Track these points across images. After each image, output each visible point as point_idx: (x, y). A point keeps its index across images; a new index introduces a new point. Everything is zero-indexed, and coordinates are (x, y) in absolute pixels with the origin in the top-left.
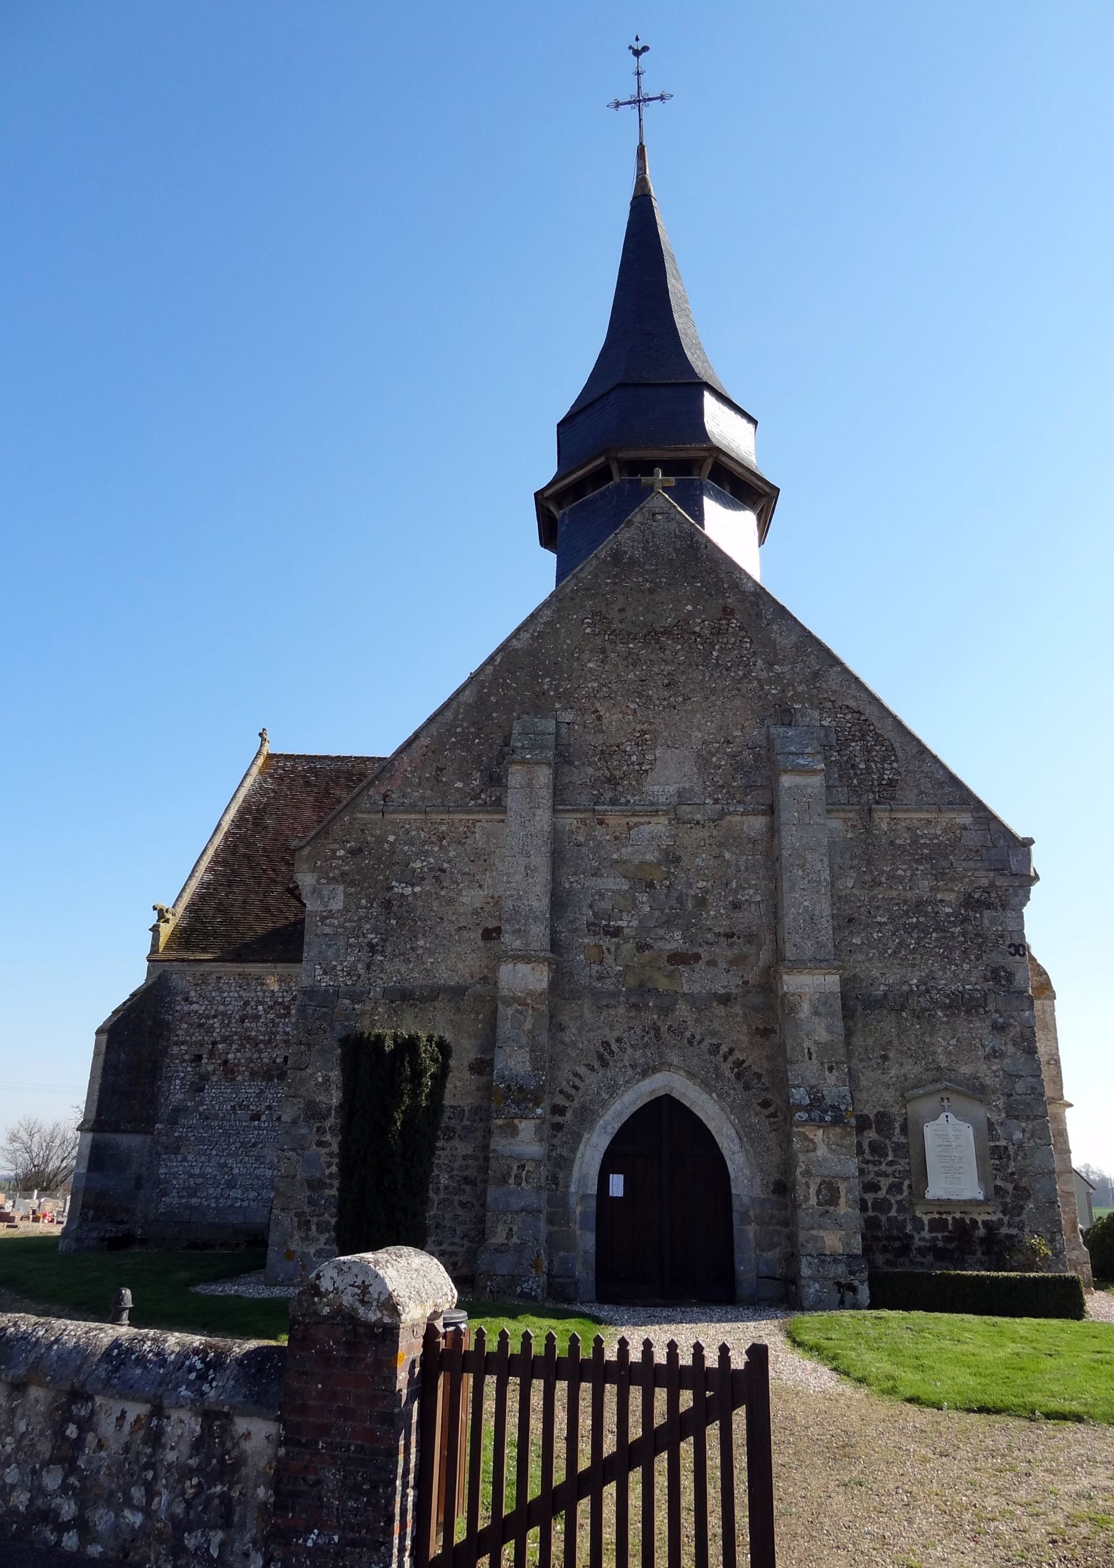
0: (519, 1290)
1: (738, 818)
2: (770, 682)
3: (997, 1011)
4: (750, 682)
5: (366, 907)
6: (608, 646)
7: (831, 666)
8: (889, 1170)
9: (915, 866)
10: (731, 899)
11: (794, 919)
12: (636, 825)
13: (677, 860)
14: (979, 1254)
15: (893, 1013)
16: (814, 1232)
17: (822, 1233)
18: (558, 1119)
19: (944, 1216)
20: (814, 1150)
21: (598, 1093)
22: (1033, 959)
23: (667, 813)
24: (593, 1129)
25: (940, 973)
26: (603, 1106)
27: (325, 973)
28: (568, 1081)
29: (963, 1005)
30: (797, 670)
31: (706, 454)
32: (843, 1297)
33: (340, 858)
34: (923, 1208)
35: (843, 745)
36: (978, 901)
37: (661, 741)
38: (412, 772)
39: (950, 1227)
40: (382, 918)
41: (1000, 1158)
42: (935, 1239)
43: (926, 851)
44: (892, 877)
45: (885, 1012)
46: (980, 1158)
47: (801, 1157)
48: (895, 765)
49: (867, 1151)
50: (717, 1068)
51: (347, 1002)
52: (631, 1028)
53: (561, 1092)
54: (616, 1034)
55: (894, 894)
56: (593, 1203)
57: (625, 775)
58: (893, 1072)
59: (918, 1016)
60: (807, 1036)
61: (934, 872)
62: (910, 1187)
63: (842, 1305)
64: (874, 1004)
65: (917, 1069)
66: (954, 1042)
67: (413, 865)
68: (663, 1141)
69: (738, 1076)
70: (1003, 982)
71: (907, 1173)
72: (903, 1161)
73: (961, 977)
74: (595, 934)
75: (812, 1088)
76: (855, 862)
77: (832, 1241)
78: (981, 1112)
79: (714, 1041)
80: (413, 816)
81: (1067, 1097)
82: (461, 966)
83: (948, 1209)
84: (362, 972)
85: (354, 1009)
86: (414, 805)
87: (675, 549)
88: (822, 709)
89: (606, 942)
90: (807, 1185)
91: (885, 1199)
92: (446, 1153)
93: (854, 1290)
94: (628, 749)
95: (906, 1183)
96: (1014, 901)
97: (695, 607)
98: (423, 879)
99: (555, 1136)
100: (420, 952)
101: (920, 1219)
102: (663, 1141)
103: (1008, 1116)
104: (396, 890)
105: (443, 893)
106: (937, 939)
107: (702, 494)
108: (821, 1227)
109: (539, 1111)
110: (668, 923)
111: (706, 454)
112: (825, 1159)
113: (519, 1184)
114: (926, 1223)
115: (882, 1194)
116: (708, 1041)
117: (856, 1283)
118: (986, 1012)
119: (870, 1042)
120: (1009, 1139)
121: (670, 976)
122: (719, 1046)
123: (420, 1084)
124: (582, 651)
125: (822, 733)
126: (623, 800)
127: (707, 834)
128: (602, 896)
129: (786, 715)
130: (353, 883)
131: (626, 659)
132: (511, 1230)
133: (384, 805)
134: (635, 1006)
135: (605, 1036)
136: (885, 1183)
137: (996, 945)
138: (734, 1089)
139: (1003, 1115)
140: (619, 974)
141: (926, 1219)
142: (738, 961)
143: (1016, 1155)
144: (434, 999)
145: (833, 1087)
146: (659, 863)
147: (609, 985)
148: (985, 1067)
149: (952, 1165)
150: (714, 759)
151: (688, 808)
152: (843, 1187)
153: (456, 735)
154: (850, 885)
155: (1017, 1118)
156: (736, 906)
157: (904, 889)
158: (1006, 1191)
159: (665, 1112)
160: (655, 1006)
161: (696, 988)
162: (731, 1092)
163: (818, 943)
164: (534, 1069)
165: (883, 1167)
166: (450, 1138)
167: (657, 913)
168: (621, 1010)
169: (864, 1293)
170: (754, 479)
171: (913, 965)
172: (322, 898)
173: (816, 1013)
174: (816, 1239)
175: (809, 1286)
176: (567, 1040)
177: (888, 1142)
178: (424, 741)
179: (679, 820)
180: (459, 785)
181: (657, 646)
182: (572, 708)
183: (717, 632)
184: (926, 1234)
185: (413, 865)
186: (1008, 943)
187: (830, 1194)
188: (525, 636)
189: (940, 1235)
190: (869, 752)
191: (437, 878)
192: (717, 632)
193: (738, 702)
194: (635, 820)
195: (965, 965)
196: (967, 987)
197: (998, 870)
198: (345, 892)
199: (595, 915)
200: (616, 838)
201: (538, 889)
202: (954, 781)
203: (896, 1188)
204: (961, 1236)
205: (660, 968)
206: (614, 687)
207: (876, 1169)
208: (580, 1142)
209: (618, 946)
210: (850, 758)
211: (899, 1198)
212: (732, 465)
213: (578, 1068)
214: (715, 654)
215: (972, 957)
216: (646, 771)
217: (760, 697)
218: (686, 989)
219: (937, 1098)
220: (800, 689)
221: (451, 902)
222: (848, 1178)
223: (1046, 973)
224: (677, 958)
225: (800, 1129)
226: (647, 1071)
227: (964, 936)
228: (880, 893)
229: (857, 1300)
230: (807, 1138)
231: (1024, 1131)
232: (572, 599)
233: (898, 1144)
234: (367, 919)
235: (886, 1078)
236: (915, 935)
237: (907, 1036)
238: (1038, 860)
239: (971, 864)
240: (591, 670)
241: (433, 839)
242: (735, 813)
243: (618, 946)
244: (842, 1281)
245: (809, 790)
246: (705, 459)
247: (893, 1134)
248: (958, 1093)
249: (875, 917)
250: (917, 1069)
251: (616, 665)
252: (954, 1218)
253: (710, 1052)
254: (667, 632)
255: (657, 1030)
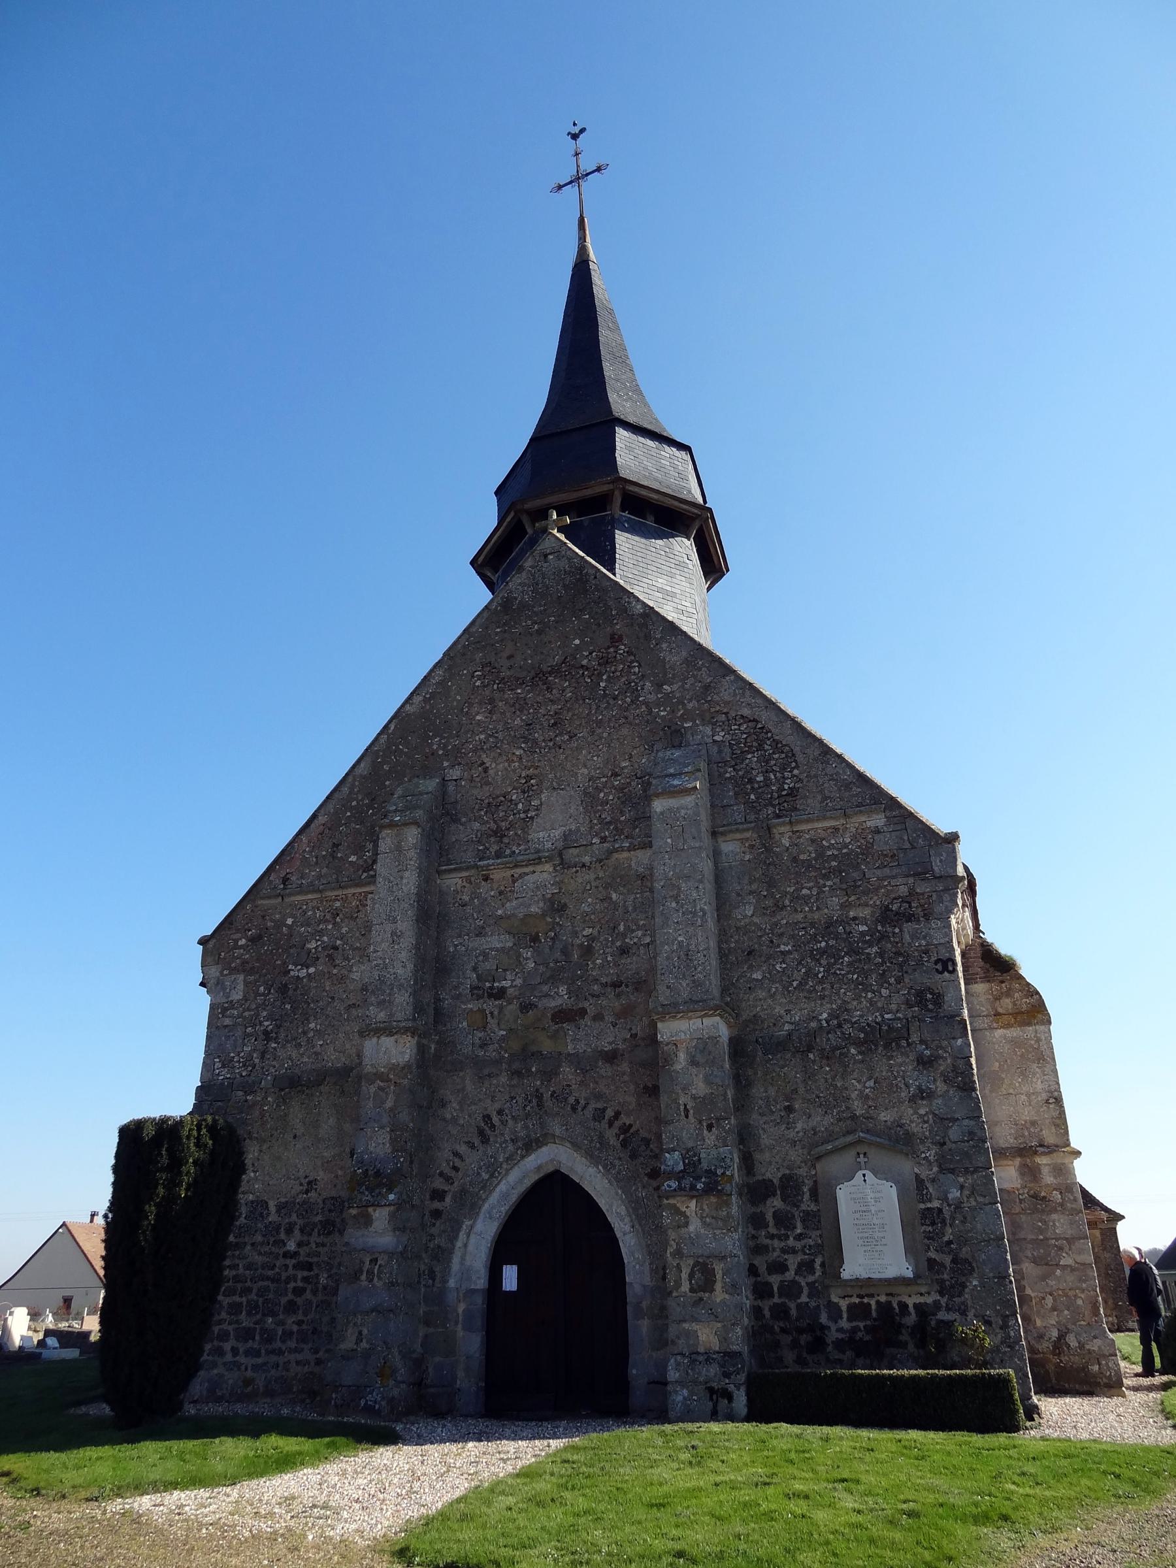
0: (363, 1402)
1: (625, 854)
2: (658, 704)
3: (922, 1042)
4: (638, 707)
5: (263, 994)
6: (497, 695)
7: (724, 676)
8: (798, 1245)
9: (822, 882)
10: (618, 944)
11: (668, 958)
12: (521, 876)
13: (563, 907)
14: (911, 1347)
15: (798, 1056)
16: (686, 1326)
17: (695, 1326)
18: (437, 1205)
19: (866, 1300)
20: (687, 1224)
21: (478, 1173)
22: (1021, 978)
23: (550, 859)
24: (478, 1214)
25: (855, 1003)
26: (483, 1188)
27: (223, 1066)
28: (448, 1161)
29: (883, 1038)
30: (687, 686)
31: (611, 487)
32: (716, 1406)
33: (241, 947)
34: (840, 1291)
35: (739, 758)
36: (897, 914)
37: (546, 784)
38: (310, 852)
39: (874, 1314)
40: (278, 1003)
41: (933, 1224)
42: (855, 1330)
43: (834, 864)
44: (796, 898)
45: (789, 1056)
46: (907, 1226)
47: (672, 1235)
48: (796, 772)
49: (771, 1223)
50: (601, 1136)
51: (240, 1093)
52: (513, 1098)
53: (441, 1174)
54: (497, 1106)
55: (800, 917)
56: (479, 1300)
57: (511, 826)
58: (799, 1126)
59: (827, 1057)
60: (683, 1089)
61: (844, 886)
62: (823, 1265)
63: (714, 1416)
64: (779, 1046)
65: (829, 1120)
66: (871, 1083)
67: (308, 946)
68: (554, 1222)
69: (624, 1144)
70: (930, 1006)
71: (819, 1249)
72: (815, 1234)
73: (879, 1005)
74: (479, 997)
75: (688, 1151)
76: (754, 887)
77: (707, 1336)
78: (908, 1167)
79: (599, 1105)
80: (310, 896)
81: (1075, 1143)
82: (348, 1046)
83: (871, 1291)
84: (257, 1061)
85: (246, 1101)
86: (312, 884)
87: (564, 586)
88: (714, 724)
89: (490, 1005)
90: (679, 1267)
91: (794, 1282)
92: (326, 1249)
93: (730, 1397)
94: (514, 797)
95: (818, 1261)
96: (939, 908)
97: (582, 641)
98: (318, 959)
99: (434, 1225)
100: (311, 1034)
101: (837, 1304)
102: (554, 1222)
103: (942, 1170)
104: (292, 973)
105: (335, 971)
106: (850, 964)
107: (614, 528)
108: (694, 1319)
109: (391, 1197)
110: (553, 978)
111: (611, 487)
112: (698, 1236)
113: (371, 1281)
114: (844, 1308)
115: (790, 1275)
116: (593, 1105)
117: (731, 1387)
118: (909, 1045)
119: (772, 1092)
120: (945, 1199)
121: (554, 1036)
122: (604, 1110)
123: (180, 1173)
124: (471, 705)
125: (715, 749)
126: (508, 852)
127: (593, 876)
128: (485, 955)
129: (675, 736)
130: (251, 971)
131: (513, 705)
132: (360, 1333)
133: (284, 889)
134: (518, 1073)
135: (486, 1109)
136: (793, 1262)
137: (920, 963)
138: (620, 1159)
139: (935, 1169)
140: (503, 1038)
141: (844, 1304)
142: (626, 1012)
143: (953, 1218)
144: (319, 1083)
145: (714, 1147)
146: (544, 915)
147: (491, 1052)
148: (911, 1111)
149: (873, 1233)
150: (602, 795)
151: (575, 851)
152: (719, 1268)
153: (351, 808)
154: (750, 913)
155: (952, 1171)
156: (624, 951)
157: (811, 910)
158: (943, 1265)
159: (555, 1189)
160: (538, 1071)
161: (581, 1047)
162: (617, 1162)
163: (694, 981)
164: (395, 1150)
165: (791, 1242)
166: (329, 1233)
167: (542, 969)
168: (503, 1079)
169: (741, 1401)
170: (676, 503)
171: (822, 998)
172: (224, 989)
173: (693, 1062)
174: (689, 1334)
175: (676, 1392)
176: (448, 1116)
177: (790, 1212)
178: (322, 819)
179: (564, 865)
180: (353, 858)
181: (545, 687)
182: (459, 764)
183: (605, 661)
184: (844, 1323)
185: (308, 946)
186: (933, 959)
187: (704, 1278)
188: (417, 699)
189: (861, 1325)
190: (767, 762)
191: (330, 957)
192: (605, 661)
193: (625, 731)
194: (519, 871)
195: (883, 991)
196: (886, 1016)
197: (920, 874)
198: (245, 981)
199: (479, 977)
200: (501, 893)
201: (404, 955)
202: (863, 780)
203: (806, 1267)
204: (884, 1324)
205: (544, 1029)
206: (500, 736)
207: (783, 1244)
208: (459, 1230)
209: (501, 1008)
210: (747, 772)
211: (811, 1279)
212: (644, 493)
213: (458, 1147)
214: (602, 684)
215: (892, 980)
216: (532, 818)
217: (647, 722)
218: (570, 1049)
219: (853, 1153)
220: (690, 706)
221: (342, 979)
222: (724, 1258)
223: (1038, 993)
224: (563, 1016)
225: (672, 1201)
226: (530, 1145)
227: (881, 956)
228: (784, 918)
229: (732, 1410)
230: (677, 1211)
231: (962, 1187)
232: (464, 655)
233: (807, 1213)
234: (263, 1006)
235: (791, 1134)
236: (824, 962)
237: (816, 1081)
238: (967, 855)
239: (887, 871)
240: (479, 722)
241: (328, 917)
242: (622, 849)
243: (501, 1008)
244: (714, 1385)
245: (683, 812)
246: (612, 491)
247: (801, 1201)
248: (879, 1146)
249: (779, 946)
250: (829, 1120)
251: (503, 713)
252: (878, 1302)
253: (594, 1119)
254: (555, 671)
255: (540, 1097)
